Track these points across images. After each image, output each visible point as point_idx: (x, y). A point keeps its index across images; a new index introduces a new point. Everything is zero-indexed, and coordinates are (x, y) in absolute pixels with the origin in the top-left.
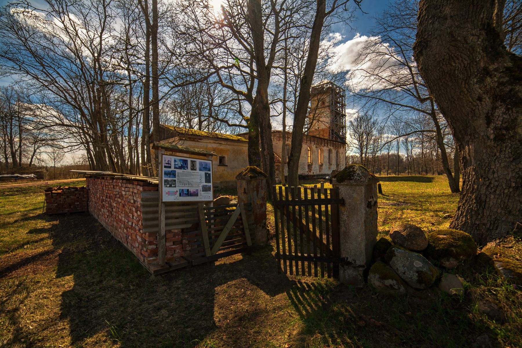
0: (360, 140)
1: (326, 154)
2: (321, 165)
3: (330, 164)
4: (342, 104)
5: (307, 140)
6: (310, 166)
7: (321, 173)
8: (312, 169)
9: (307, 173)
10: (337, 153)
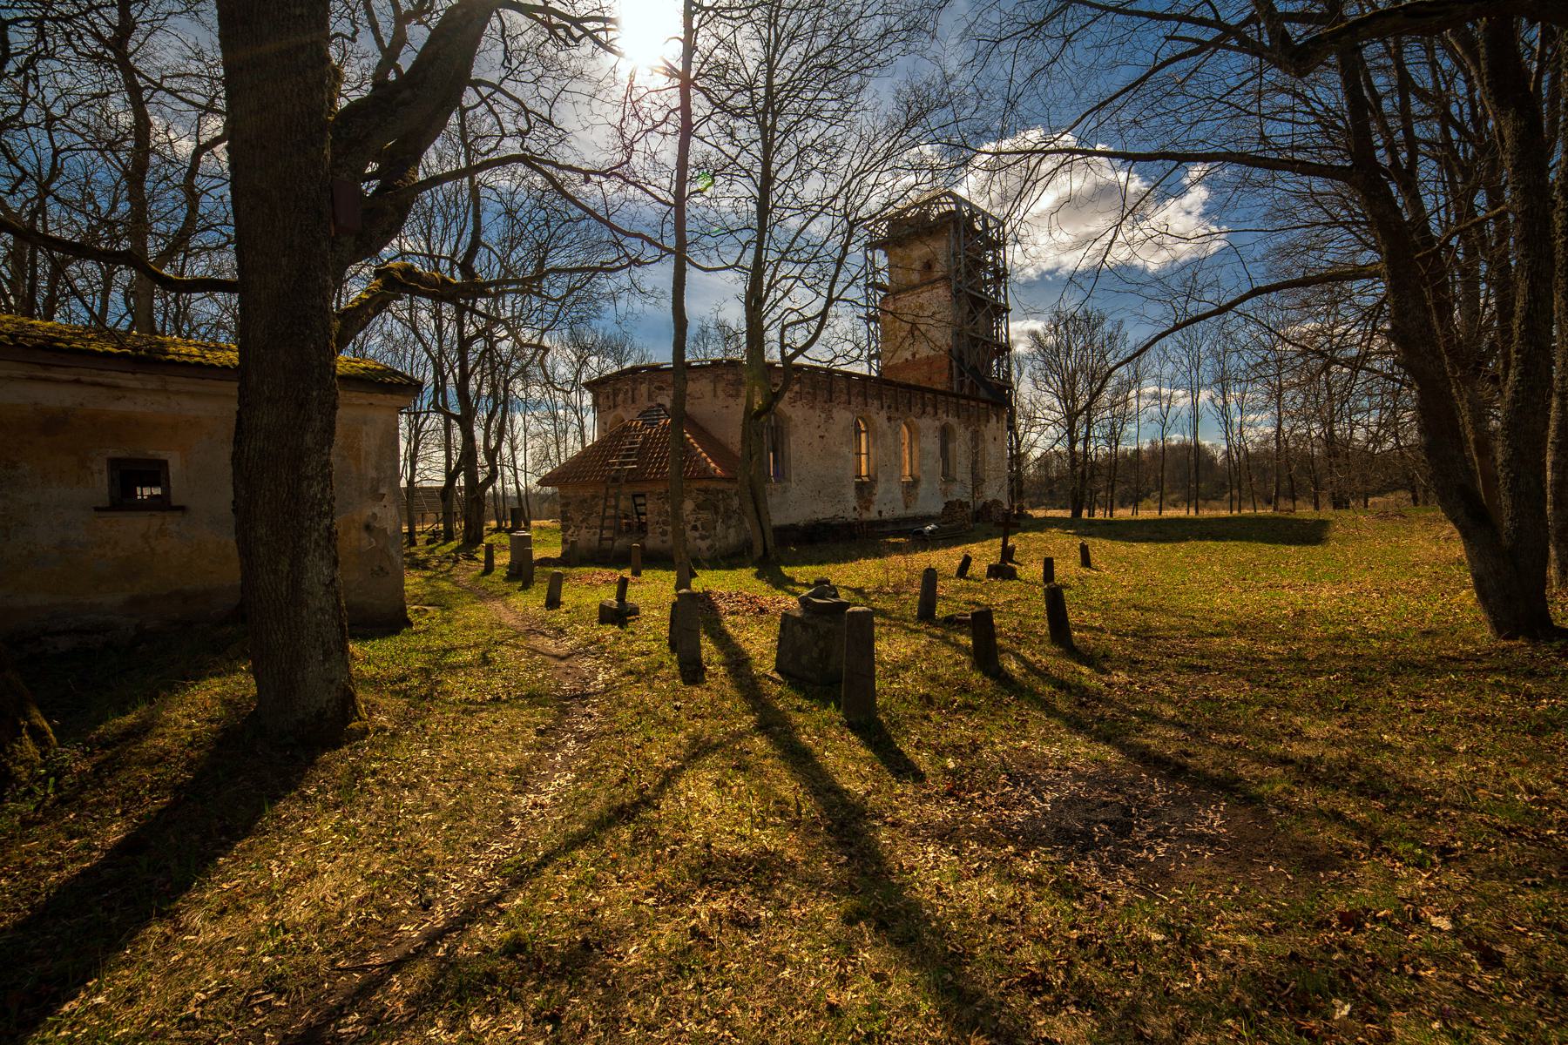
0: (1067, 395)
1: (931, 443)
2: (915, 483)
3: (948, 477)
4: (996, 271)
5: (849, 394)
6: (864, 489)
7: (910, 512)
8: (875, 498)
9: (855, 515)
10: (976, 438)
